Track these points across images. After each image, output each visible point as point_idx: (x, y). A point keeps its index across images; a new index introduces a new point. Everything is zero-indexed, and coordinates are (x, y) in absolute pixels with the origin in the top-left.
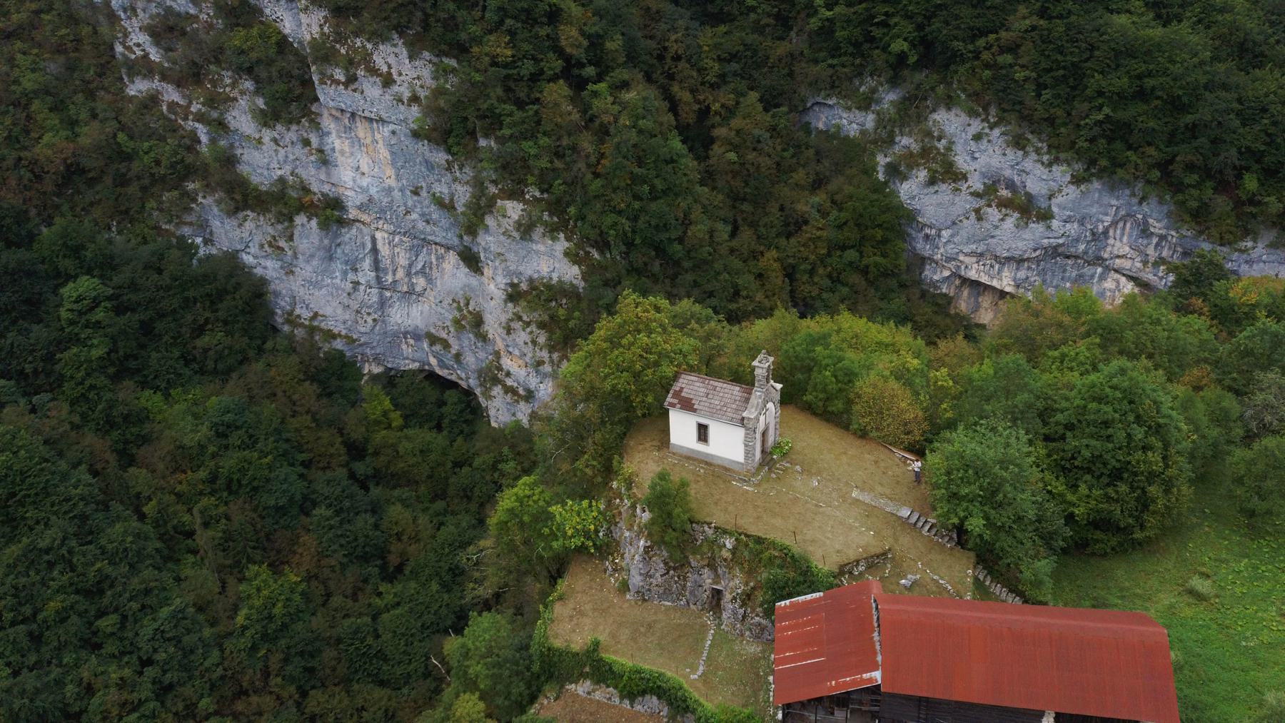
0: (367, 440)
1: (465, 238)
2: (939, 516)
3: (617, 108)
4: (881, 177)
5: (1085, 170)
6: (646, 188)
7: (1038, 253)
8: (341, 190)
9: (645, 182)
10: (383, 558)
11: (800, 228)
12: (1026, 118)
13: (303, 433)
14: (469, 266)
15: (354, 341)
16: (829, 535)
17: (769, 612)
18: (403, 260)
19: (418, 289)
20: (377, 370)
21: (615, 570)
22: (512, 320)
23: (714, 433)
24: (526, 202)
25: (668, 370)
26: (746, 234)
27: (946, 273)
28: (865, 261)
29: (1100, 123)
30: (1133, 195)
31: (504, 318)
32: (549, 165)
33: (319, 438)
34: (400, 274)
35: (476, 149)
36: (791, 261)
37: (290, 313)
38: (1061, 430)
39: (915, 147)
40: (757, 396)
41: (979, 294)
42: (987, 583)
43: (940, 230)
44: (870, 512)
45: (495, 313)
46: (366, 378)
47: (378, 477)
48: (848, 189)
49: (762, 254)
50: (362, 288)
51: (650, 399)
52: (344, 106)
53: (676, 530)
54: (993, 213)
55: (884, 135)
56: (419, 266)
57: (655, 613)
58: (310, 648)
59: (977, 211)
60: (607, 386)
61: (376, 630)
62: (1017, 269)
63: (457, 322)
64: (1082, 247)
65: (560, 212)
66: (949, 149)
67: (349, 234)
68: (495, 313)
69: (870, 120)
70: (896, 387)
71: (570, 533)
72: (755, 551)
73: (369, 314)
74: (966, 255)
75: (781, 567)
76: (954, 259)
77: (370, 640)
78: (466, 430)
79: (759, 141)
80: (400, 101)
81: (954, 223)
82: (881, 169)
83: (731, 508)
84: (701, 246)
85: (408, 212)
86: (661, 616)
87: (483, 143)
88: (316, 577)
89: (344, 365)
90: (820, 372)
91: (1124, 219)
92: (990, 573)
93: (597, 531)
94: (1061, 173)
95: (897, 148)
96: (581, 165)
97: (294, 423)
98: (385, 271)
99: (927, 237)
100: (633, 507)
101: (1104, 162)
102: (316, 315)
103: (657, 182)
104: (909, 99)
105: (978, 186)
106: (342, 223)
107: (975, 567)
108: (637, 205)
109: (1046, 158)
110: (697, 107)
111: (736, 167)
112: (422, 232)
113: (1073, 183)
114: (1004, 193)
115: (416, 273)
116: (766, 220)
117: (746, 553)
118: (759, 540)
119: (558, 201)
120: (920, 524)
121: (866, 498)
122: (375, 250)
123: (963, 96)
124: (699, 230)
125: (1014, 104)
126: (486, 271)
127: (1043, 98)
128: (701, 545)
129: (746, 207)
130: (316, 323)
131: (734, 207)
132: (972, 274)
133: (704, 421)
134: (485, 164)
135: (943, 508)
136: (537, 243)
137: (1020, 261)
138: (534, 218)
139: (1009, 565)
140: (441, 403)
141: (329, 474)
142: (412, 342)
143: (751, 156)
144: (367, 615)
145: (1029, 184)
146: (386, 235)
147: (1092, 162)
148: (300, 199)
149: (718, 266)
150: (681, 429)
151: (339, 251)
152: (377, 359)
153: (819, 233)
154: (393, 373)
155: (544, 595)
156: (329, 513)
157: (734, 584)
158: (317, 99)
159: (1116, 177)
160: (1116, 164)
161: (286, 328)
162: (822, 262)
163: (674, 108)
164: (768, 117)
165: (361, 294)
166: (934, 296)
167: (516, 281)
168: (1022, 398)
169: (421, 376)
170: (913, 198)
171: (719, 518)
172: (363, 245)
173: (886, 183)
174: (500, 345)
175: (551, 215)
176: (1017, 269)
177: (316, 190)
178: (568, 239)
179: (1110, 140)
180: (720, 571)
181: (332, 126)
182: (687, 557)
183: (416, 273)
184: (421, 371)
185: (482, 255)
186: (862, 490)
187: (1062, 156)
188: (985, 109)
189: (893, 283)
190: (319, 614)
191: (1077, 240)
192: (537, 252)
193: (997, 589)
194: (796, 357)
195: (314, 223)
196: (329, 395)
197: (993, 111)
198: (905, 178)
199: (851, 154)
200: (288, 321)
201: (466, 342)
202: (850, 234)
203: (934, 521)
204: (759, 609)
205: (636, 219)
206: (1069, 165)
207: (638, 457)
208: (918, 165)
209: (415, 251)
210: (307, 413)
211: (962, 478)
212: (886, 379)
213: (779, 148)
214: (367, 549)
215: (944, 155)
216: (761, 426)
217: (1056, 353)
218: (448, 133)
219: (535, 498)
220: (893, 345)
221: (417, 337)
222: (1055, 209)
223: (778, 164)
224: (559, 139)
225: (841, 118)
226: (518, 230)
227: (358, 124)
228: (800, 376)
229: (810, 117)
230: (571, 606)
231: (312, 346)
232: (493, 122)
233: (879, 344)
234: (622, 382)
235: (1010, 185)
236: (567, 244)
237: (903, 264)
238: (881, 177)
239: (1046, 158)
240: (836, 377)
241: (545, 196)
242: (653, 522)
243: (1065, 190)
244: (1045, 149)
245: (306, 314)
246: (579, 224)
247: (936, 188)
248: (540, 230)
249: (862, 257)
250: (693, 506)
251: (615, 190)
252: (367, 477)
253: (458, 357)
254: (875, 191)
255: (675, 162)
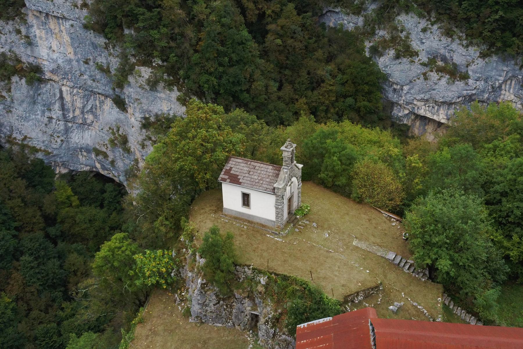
0: (56, 214)
1: (116, 90)
2: (416, 258)
3: (208, 10)
4: (367, 54)
5: (488, 49)
6: (227, 59)
7: (460, 99)
8: (40, 61)
9: (226, 56)
10: (65, 286)
11: (319, 85)
12: (453, 18)
13: (16, 210)
14: (119, 108)
15: (49, 153)
16: (337, 273)
17: (292, 332)
18: (79, 104)
19: (89, 121)
20: (64, 171)
21: (182, 301)
22: (145, 140)
23: (254, 200)
24: (153, 67)
25: (221, 154)
26: (288, 89)
27: (407, 112)
28: (358, 104)
29: (496, 21)
30: (516, 64)
31: (140, 138)
32: (166, 45)
33: (27, 213)
34: (77, 112)
35: (122, 35)
36: (314, 104)
37: (10, 136)
38: (498, 197)
39: (388, 37)
40: (284, 172)
41: (425, 125)
42: (451, 307)
43: (402, 86)
44: (366, 255)
45: (135, 135)
46: (57, 176)
47: (63, 236)
48: (348, 62)
49: (297, 100)
50: (54, 121)
51: (208, 176)
52: (41, 9)
53: (225, 272)
54: (434, 76)
55: (369, 29)
56: (89, 108)
57: (210, 332)
58: (16, 344)
59: (424, 74)
60: (177, 167)
61: (59, 331)
62: (448, 109)
63: (112, 141)
64: (486, 96)
65: (176, 73)
66: (407, 37)
67: (45, 88)
68: (135, 135)
69: (360, 21)
70: (383, 167)
71: (147, 274)
72: (282, 286)
73: (58, 137)
74: (418, 101)
75: (301, 298)
76: (411, 103)
77: (55, 338)
78: (118, 208)
79: (294, 33)
80: (76, 6)
81: (411, 82)
82: (367, 50)
83: (265, 254)
84: (260, 95)
85: (81, 75)
86: (214, 335)
87: (127, 32)
88: (22, 299)
89: (43, 168)
90: (330, 157)
91: (511, 79)
92: (453, 299)
93: (169, 274)
94: (474, 51)
95: (377, 38)
96: (187, 45)
97: (10, 203)
98: (68, 110)
99: (395, 90)
100: (194, 254)
101: (499, 44)
102: (26, 137)
103: (233, 55)
104: (383, 8)
105: (425, 60)
106: (41, 81)
107: (443, 296)
108: (221, 69)
109: (465, 42)
110: (257, 12)
111: (281, 48)
112: (90, 87)
113: (481, 57)
114: (440, 63)
115: (87, 112)
116: (298, 80)
117: (275, 288)
118: (285, 278)
119: (173, 67)
120: (402, 264)
121: (363, 245)
122: (62, 98)
123: (415, 6)
124: (259, 85)
125: (446, 10)
126: (129, 110)
127: (463, 7)
128: (243, 282)
129: (287, 72)
130: (25, 143)
131: (280, 72)
132: (422, 112)
133: (246, 191)
134: (128, 44)
135: (419, 252)
136: (160, 92)
137: (450, 104)
138: (158, 77)
139: (467, 294)
140: (103, 191)
141: (31, 235)
142: (85, 154)
143: (290, 41)
144: (54, 322)
145: (455, 58)
146: (68, 89)
147: (492, 45)
148: (14, 67)
149: (271, 107)
150: (231, 197)
151: (39, 98)
152: (64, 165)
153: (331, 88)
154: (74, 173)
155: (129, 320)
156: (31, 259)
157: (267, 310)
158: (24, 5)
159: (506, 54)
160: (506, 45)
161: (7, 146)
162: (333, 104)
163: (244, 12)
164: (300, 19)
165: (53, 125)
166: (399, 125)
167: (147, 116)
168: (471, 174)
169: (92, 175)
170: (386, 67)
171: (256, 261)
172: (55, 95)
173: (370, 58)
174: (138, 155)
175: (169, 75)
176: (448, 109)
177: (24, 61)
178: (179, 90)
179: (503, 31)
180: (257, 301)
181: (34, 22)
182: (232, 291)
183: (87, 112)
184: (91, 172)
185: (127, 100)
186: (360, 240)
187: (474, 41)
188: (429, 13)
189: (375, 117)
190: (23, 322)
191: (483, 91)
192: (160, 98)
193: (459, 311)
194: (313, 147)
195: (23, 81)
196: (34, 186)
197: (433, 14)
198: (381, 55)
199: (349, 41)
200: (8, 142)
201: (118, 154)
202: (349, 88)
203: (412, 262)
204: (285, 330)
205: (220, 78)
206: (478, 46)
207: (200, 218)
208: (389, 47)
209: (86, 98)
210: (19, 197)
211: (433, 230)
212: (375, 162)
213: (306, 37)
214: (55, 281)
215: (404, 41)
216: (288, 194)
217: (491, 145)
218: (105, 25)
219: (123, 249)
220: (379, 142)
221: (88, 151)
222: (470, 73)
223: (306, 47)
224: (173, 29)
225: (343, 20)
226: (148, 85)
227: (51, 20)
228: (316, 160)
229: (325, 20)
230: (148, 327)
231: (23, 156)
232: (132, 19)
233: (370, 141)
234: (188, 163)
235: (444, 59)
236: (178, 94)
237: (380, 105)
238: (367, 54)
239: (465, 42)
240: (341, 161)
241: (165, 64)
242: (207, 265)
243: (476, 62)
244: (464, 37)
245: (19, 137)
246: (186, 81)
247: (400, 61)
248: (162, 84)
249: (356, 101)
250: (237, 253)
251: (208, 60)
252: (57, 237)
253: (113, 163)
254: (364, 63)
255: (243, 43)
